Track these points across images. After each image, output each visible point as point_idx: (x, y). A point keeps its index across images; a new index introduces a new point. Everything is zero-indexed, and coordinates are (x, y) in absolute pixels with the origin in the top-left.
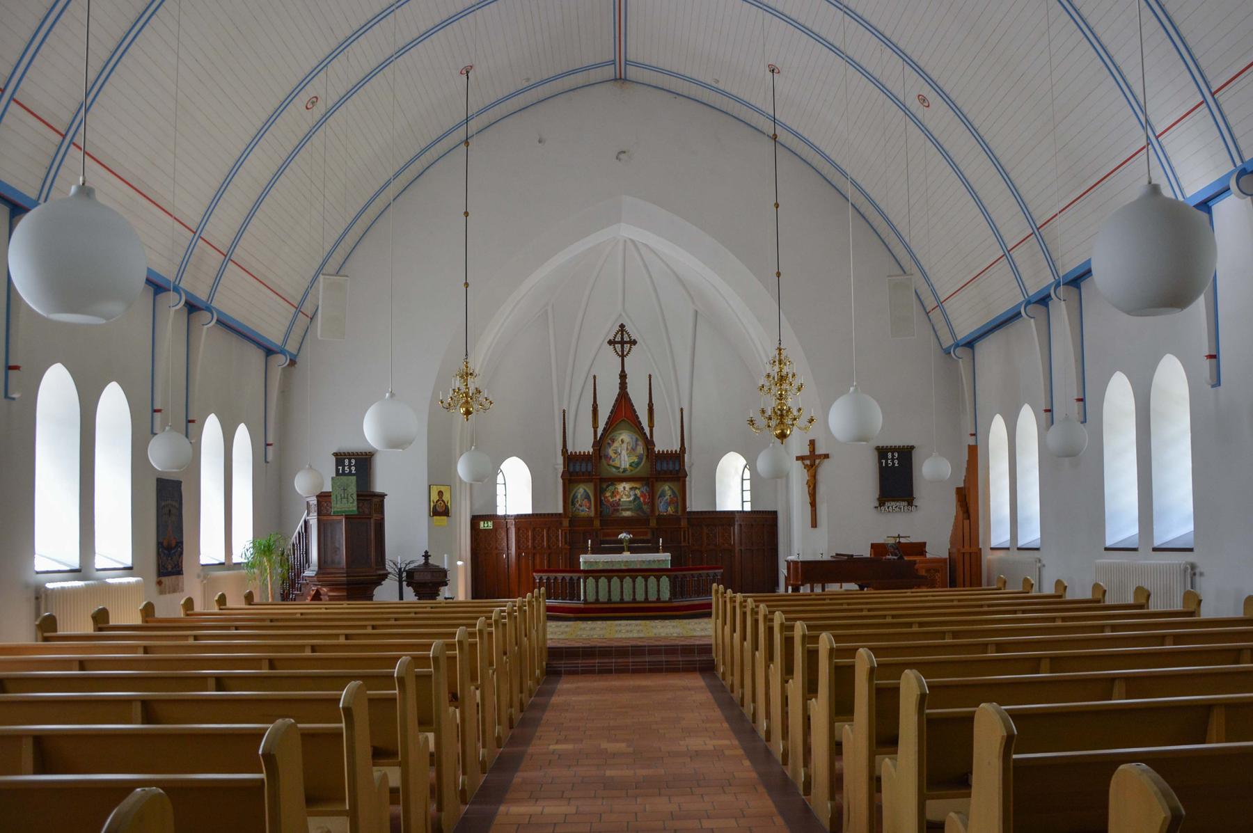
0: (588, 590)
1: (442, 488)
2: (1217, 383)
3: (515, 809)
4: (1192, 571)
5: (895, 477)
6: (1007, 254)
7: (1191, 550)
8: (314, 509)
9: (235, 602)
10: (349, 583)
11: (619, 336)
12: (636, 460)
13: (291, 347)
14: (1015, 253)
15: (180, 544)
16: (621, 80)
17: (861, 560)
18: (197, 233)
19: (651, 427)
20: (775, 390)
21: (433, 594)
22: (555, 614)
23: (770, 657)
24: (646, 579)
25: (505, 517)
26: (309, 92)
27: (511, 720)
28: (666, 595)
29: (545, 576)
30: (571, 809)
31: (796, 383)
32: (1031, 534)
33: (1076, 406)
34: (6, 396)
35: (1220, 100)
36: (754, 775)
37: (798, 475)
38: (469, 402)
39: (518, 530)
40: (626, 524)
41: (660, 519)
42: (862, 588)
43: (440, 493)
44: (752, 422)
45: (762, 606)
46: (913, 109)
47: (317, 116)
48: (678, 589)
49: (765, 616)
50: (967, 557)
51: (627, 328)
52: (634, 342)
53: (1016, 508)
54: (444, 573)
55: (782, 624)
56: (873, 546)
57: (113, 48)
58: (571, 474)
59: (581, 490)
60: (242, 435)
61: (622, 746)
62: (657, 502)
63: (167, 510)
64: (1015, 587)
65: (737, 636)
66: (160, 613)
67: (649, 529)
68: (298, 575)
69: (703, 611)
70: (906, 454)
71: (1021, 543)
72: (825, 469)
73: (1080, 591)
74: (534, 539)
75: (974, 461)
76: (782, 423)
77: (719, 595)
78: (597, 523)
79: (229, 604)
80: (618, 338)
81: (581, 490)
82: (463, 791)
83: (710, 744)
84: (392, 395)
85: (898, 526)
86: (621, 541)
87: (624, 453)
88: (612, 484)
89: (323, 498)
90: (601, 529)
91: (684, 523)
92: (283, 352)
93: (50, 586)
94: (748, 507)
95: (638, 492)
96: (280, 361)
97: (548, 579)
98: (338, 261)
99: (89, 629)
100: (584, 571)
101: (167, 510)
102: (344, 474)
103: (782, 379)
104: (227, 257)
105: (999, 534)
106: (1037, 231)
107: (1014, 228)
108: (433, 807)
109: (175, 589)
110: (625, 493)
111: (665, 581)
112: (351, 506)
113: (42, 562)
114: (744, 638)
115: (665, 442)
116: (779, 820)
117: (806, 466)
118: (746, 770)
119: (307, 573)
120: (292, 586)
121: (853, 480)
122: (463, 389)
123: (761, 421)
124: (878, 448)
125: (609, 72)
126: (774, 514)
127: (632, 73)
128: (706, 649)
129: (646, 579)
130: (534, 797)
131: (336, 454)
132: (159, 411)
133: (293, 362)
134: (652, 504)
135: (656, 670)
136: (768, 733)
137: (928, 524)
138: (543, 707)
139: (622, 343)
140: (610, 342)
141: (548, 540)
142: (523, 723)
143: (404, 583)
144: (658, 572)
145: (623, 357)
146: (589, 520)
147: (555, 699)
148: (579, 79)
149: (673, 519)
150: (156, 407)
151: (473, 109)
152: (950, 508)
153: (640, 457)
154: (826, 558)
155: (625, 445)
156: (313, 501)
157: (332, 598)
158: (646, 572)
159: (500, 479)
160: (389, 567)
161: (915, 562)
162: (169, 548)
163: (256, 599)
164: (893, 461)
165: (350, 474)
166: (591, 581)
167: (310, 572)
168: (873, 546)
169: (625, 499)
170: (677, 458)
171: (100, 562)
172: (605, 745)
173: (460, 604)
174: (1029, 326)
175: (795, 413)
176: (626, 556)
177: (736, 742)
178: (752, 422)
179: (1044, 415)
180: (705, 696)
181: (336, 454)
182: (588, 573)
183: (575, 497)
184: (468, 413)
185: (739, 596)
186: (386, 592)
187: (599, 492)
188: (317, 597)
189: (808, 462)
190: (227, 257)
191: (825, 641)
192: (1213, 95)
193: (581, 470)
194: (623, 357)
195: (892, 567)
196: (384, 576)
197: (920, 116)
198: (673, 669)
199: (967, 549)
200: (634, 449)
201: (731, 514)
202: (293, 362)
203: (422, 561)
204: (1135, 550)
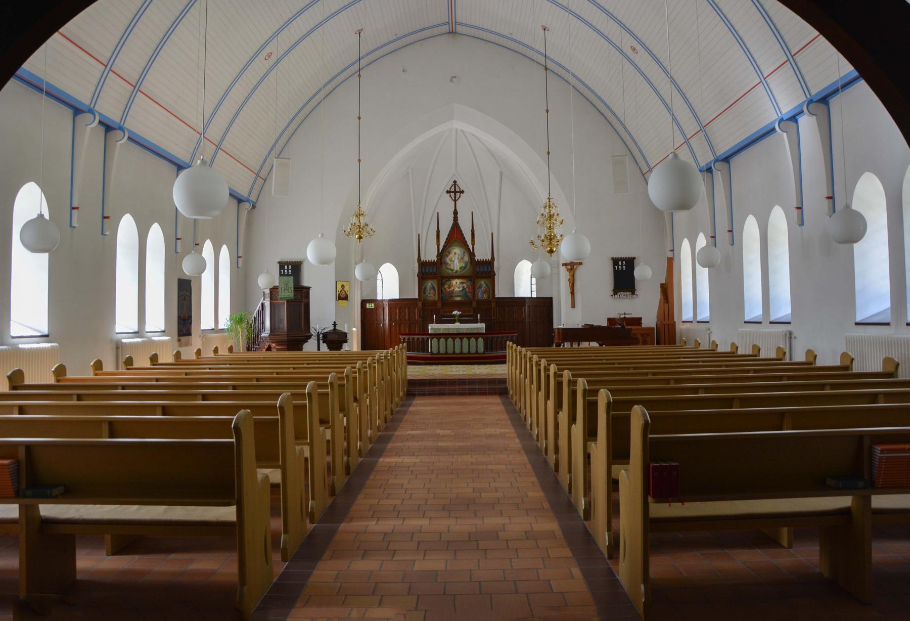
0: (433, 346)
1: (344, 283)
2: (802, 224)
3: (388, 460)
4: (790, 336)
5: (624, 278)
6: (687, 141)
7: (789, 323)
8: (268, 296)
9: (223, 352)
10: (288, 341)
12: (464, 265)
13: (253, 198)
14: (691, 141)
15: (190, 317)
16: (453, 33)
17: (599, 328)
18: (202, 134)
20: (547, 224)
21: (339, 348)
22: (412, 361)
23: (539, 389)
24: (469, 339)
25: (382, 301)
26: (267, 50)
27: (386, 418)
28: (481, 349)
29: (407, 337)
30: (418, 460)
31: (559, 219)
32: (705, 313)
33: (728, 235)
34: (71, 226)
35: (797, 60)
36: (520, 446)
37: (564, 274)
38: (360, 231)
39: (390, 309)
40: (457, 306)
41: (479, 302)
42: (601, 345)
43: (343, 286)
44: (532, 243)
45: (543, 360)
46: (628, 54)
47: (271, 63)
48: (488, 346)
49: (545, 367)
50: (667, 328)
52: (462, 192)
53: (695, 296)
54: (345, 335)
55: (555, 373)
56: (609, 320)
57: (161, 36)
58: (423, 274)
59: (429, 284)
60: (225, 251)
61: (449, 432)
62: (477, 291)
63: (184, 294)
64: (691, 345)
65: (518, 371)
66: (184, 357)
67: (472, 308)
68: (258, 336)
69: (501, 360)
70: (630, 263)
71: (699, 318)
72: (580, 272)
73: (828, 358)
75: (671, 264)
76: (551, 243)
77: (512, 349)
78: (439, 305)
79: (220, 353)
82: (360, 450)
83: (499, 431)
84: (322, 235)
85: (624, 307)
86: (454, 316)
87: (456, 261)
89: (274, 291)
90: (441, 308)
91: (493, 305)
92: (248, 201)
93: (124, 341)
94: (534, 295)
96: (247, 206)
98: (280, 148)
99: (148, 364)
100: (431, 334)
101: (184, 294)
102: (284, 275)
103: (551, 216)
104: (218, 147)
105: (687, 314)
106: (703, 129)
107: (690, 127)
108: (345, 458)
109: (188, 344)
110: (457, 285)
111: (481, 340)
112: (290, 294)
113: (119, 328)
114: (521, 373)
115: (482, 254)
116: (529, 466)
117: (568, 270)
118: (516, 443)
119: (263, 335)
120: (254, 343)
121: (598, 277)
122: (357, 224)
123: (538, 243)
124: (613, 259)
125: (446, 29)
127: (460, 29)
128: (503, 381)
129: (469, 339)
130: (397, 455)
131: (279, 263)
132: (77, 208)
133: (254, 207)
135: (472, 393)
136: (531, 425)
137: (643, 307)
138: (405, 413)
139: (455, 192)
140: (448, 192)
142: (392, 421)
143: (321, 342)
144: (476, 335)
145: (455, 201)
147: (411, 409)
148: (428, 33)
149: (487, 302)
150: (74, 206)
151: (363, 53)
152: (657, 295)
153: (466, 264)
154: (580, 326)
156: (268, 292)
157: (278, 350)
158: (469, 335)
159: (379, 277)
160: (312, 331)
161: (631, 329)
162: (184, 320)
163: (234, 350)
164: (622, 267)
165: (288, 275)
166: (435, 340)
167: (265, 334)
168: (609, 320)
169: (457, 289)
170: (490, 264)
171: (148, 328)
172: (438, 431)
173: (356, 353)
175: (559, 237)
176: (457, 325)
177: (513, 430)
178: (532, 243)
179: (710, 239)
180: (501, 408)
181: (279, 263)
182: (433, 335)
183: (425, 288)
184: (360, 238)
185: (524, 349)
186: (310, 347)
187: (441, 285)
188: (269, 349)
190: (218, 147)
191: (581, 383)
192: (792, 57)
193: (430, 272)
194: (455, 201)
195: (621, 332)
196: (310, 337)
197: (632, 58)
198: (483, 393)
199: (666, 322)
200: (462, 258)
201: (523, 300)
202: (254, 207)
203: (332, 328)
204: (760, 323)
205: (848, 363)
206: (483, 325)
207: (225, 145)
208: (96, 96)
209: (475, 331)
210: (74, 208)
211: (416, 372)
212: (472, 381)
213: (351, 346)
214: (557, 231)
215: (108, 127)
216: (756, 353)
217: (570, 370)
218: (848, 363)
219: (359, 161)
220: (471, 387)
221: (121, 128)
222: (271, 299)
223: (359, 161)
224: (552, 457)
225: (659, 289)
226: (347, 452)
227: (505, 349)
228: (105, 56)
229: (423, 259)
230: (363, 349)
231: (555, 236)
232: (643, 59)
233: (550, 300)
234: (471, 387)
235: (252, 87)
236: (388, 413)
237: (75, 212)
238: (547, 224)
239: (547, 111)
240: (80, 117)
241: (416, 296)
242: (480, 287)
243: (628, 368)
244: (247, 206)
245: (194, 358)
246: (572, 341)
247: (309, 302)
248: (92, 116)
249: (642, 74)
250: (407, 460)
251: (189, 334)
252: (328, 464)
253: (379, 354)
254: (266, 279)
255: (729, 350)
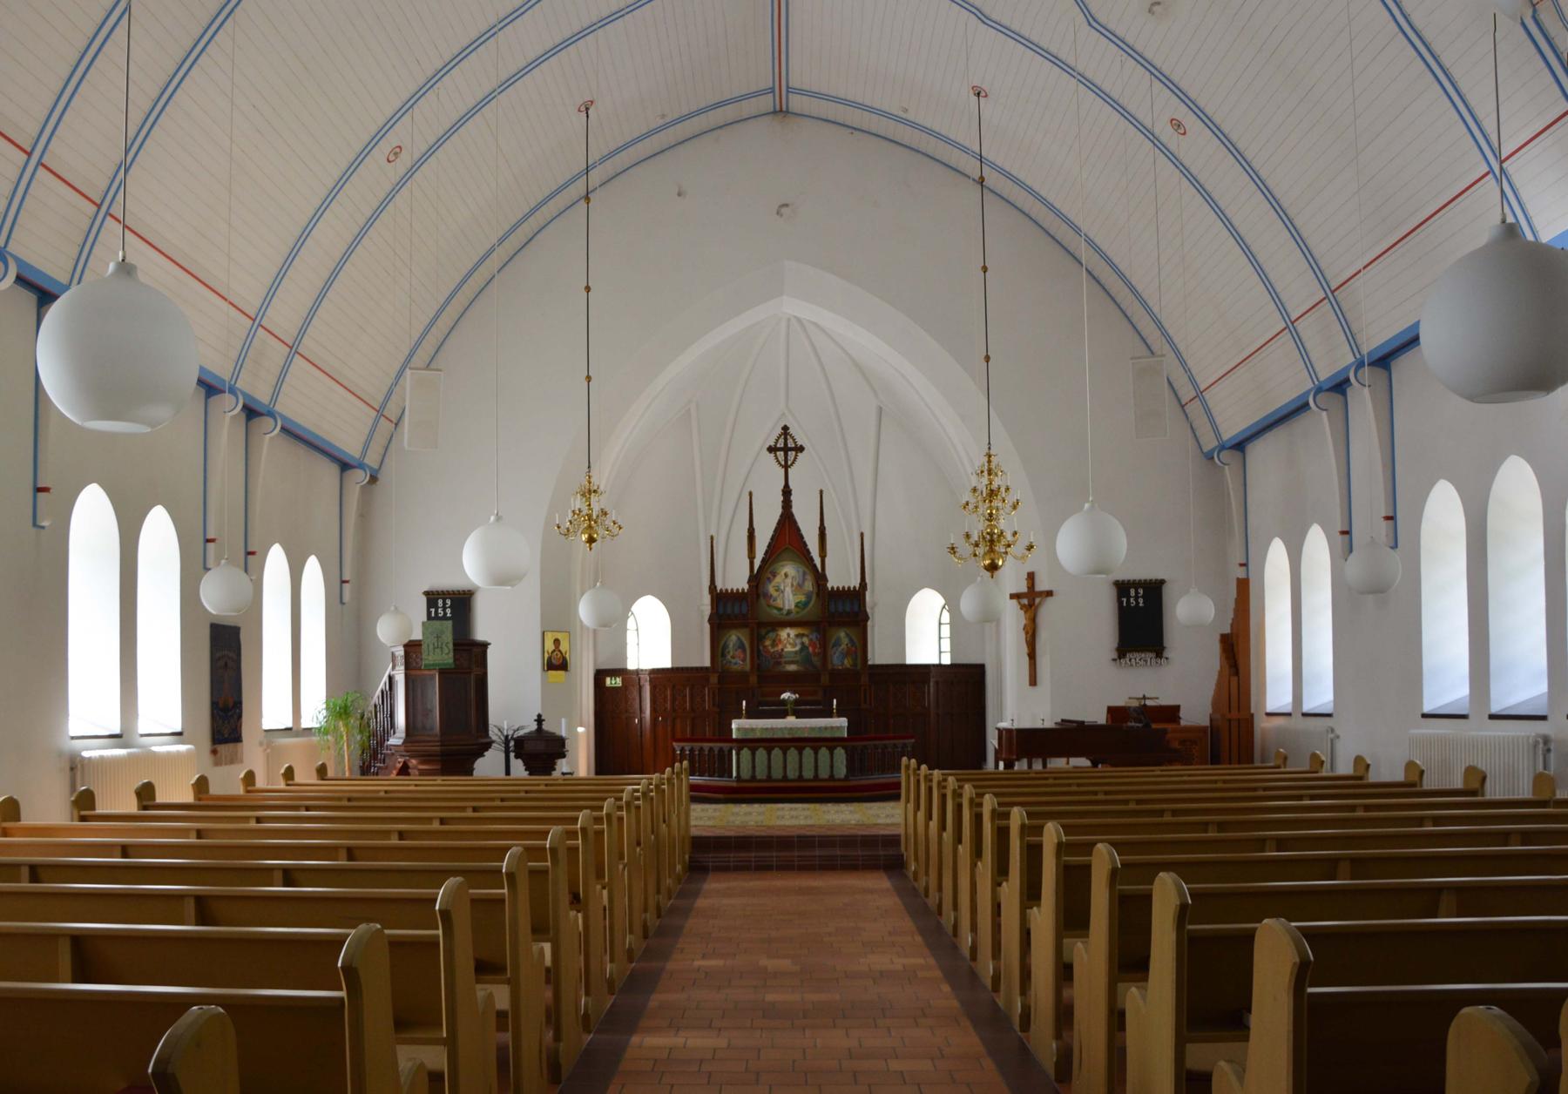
1: (559, 636)
5: (1140, 619)
7: (1544, 718)
12: (802, 598)
13: (372, 460)
14: (1300, 325)
16: (781, 112)
17: (1094, 729)
20: (984, 509)
22: (701, 795)
24: (831, 750)
25: (637, 672)
26: (392, 140)
28: (841, 770)
29: (687, 746)
30: (722, 1042)
31: (1010, 499)
32: (1320, 695)
34: (35, 524)
36: (956, 1003)
37: (1012, 618)
38: (592, 527)
40: (790, 681)
41: (836, 675)
42: (1095, 764)
44: (953, 549)
47: (402, 171)
51: (791, 431)
52: (800, 449)
53: (1300, 664)
54: (561, 741)
55: (993, 811)
57: (90, 32)
59: (733, 637)
60: (313, 569)
61: (785, 964)
63: (223, 659)
65: (934, 824)
66: (215, 789)
67: (818, 687)
69: (889, 793)
70: (1153, 590)
71: (1308, 706)
72: (1048, 612)
73: (1388, 770)
74: (674, 699)
76: (992, 550)
77: (910, 771)
78: (753, 680)
81: (734, 638)
82: (586, 1017)
83: (899, 963)
84: (498, 518)
86: (784, 702)
87: (788, 590)
88: (774, 630)
89: (412, 648)
90: (758, 686)
92: (361, 466)
93: (86, 754)
94: (946, 660)
95: (805, 640)
96: (360, 477)
97: (692, 750)
98: (429, 350)
99: (131, 806)
101: (223, 659)
102: (437, 618)
103: (992, 494)
104: (293, 349)
105: (1276, 694)
106: (1331, 294)
107: (1300, 290)
109: (234, 759)
110: (789, 640)
111: (840, 754)
112: (446, 657)
114: (943, 827)
115: (841, 575)
116: (988, 1063)
117: (1023, 607)
119: (393, 741)
120: (374, 756)
121: (1084, 624)
122: (585, 511)
123: (965, 549)
125: (767, 103)
127: (796, 102)
128: (893, 841)
129: (831, 750)
131: (427, 593)
133: (374, 479)
134: (824, 656)
135: (828, 866)
137: (1183, 682)
139: (786, 449)
140: (771, 449)
142: (661, 932)
143: (512, 755)
144: (831, 742)
145: (786, 467)
146: (742, 676)
147: (701, 903)
153: (809, 596)
154: (1049, 724)
155: (789, 581)
156: (400, 652)
157: (422, 773)
159: (631, 623)
160: (493, 733)
161: (1165, 732)
162: (226, 709)
163: (330, 773)
164: (1137, 600)
165: (445, 618)
166: (746, 753)
167: (396, 740)
168: (1111, 710)
169: (789, 649)
170: (856, 596)
171: (143, 726)
172: (764, 962)
174: (1320, 422)
175: (1009, 537)
176: (791, 721)
177: (932, 961)
178: (953, 549)
179: (1339, 538)
180: (892, 901)
181: (427, 593)
182: (742, 743)
183: (725, 646)
184: (591, 540)
186: (489, 765)
187: (757, 641)
188: (404, 770)
189: (1025, 601)
190: (293, 349)
193: (734, 613)
194: (786, 467)
195: (1135, 735)
196: (488, 746)
197: (1173, 148)
198: (851, 866)
200: (800, 586)
202: (374, 479)
203: (534, 727)
205: (1416, 778)
206: (843, 722)
207: (308, 345)
208: (236, 374)
209: (827, 735)
210: (208, 541)
211: (709, 818)
212: (826, 841)
213: (575, 763)
214: (1004, 524)
215: (251, 412)
216: (1476, 785)
217: (996, 795)
218: (1416, 778)
219: (589, 378)
220: (825, 852)
221: (271, 414)
222: (407, 668)
223: (589, 378)
224: (1044, 1046)
225: (1216, 648)
226: (553, 1016)
227: (898, 770)
228: (96, 187)
229: (719, 585)
230: (597, 773)
231: (1001, 534)
232: (1198, 148)
233: (979, 670)
234: (825, 852)
235: (362, 221)
236: (650, 917)
237: (211, 546)
238: (984, 509)
239: (985, 269)
240: (215, 399)
241: (707, 662)
242: (838, 643)
243: (1205, 826)
244: (360, 477)
245: (241, 791)
246: (1030, 755)
247: (485, 674)
248: (271, 421)
249: (1194, 181)
250: (696, 1041)
251: (237, 738)
252: (502, 1050)
253: (635, 785)
254: (398, 624)
255: (1399, 777)
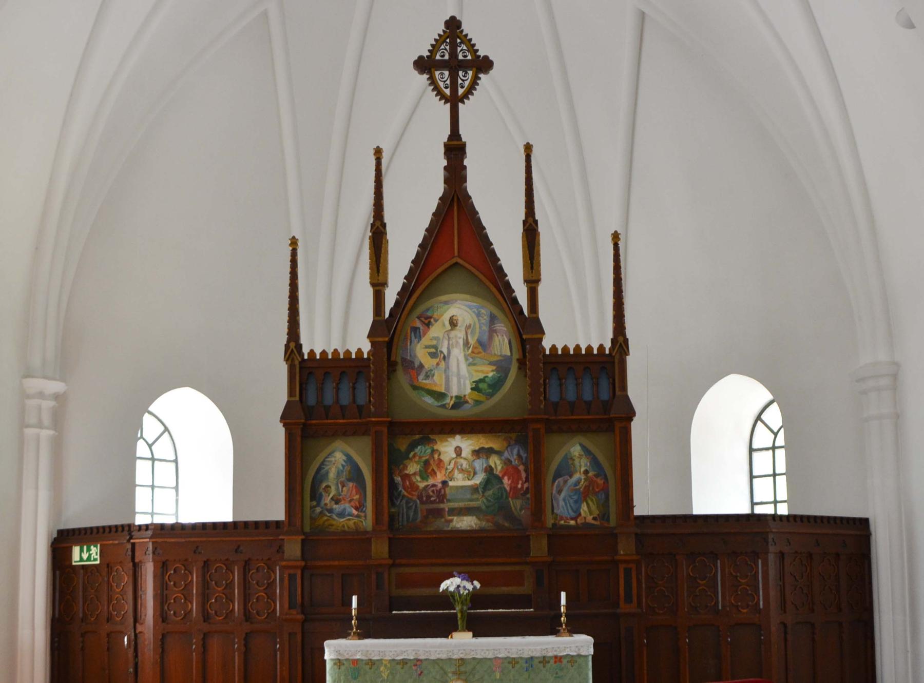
11: (445, 47)
12: (489, 372)
19: (532, 282)
39: (162, 567)
40: (462, 551)
41: (560, 537)
51: (466, 28)
58: (309, 412)
59: (338, 457)
62: (550, 488)
78: (380, 549)
80: (443, 54)
81: (339, 458)
86: (447, 600)
87: (458, 355)
88: (426, 440)
91: (625, 549)
94: (783, 510)
95: (496, 462)
110: (460, 463)
115: (572, 322)
126: (857, 532)
141: (246, 598)
146: (358, 540)
149: (596, 538)
153: (502, 367)
155: (459, 334)
169: (459, 481)
170: (607, 365)
176: (463, 642)
193: (333, 403)
194: (454, 101)
200: (484, 345)
